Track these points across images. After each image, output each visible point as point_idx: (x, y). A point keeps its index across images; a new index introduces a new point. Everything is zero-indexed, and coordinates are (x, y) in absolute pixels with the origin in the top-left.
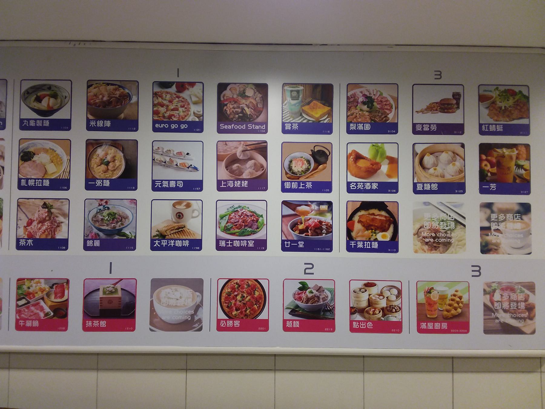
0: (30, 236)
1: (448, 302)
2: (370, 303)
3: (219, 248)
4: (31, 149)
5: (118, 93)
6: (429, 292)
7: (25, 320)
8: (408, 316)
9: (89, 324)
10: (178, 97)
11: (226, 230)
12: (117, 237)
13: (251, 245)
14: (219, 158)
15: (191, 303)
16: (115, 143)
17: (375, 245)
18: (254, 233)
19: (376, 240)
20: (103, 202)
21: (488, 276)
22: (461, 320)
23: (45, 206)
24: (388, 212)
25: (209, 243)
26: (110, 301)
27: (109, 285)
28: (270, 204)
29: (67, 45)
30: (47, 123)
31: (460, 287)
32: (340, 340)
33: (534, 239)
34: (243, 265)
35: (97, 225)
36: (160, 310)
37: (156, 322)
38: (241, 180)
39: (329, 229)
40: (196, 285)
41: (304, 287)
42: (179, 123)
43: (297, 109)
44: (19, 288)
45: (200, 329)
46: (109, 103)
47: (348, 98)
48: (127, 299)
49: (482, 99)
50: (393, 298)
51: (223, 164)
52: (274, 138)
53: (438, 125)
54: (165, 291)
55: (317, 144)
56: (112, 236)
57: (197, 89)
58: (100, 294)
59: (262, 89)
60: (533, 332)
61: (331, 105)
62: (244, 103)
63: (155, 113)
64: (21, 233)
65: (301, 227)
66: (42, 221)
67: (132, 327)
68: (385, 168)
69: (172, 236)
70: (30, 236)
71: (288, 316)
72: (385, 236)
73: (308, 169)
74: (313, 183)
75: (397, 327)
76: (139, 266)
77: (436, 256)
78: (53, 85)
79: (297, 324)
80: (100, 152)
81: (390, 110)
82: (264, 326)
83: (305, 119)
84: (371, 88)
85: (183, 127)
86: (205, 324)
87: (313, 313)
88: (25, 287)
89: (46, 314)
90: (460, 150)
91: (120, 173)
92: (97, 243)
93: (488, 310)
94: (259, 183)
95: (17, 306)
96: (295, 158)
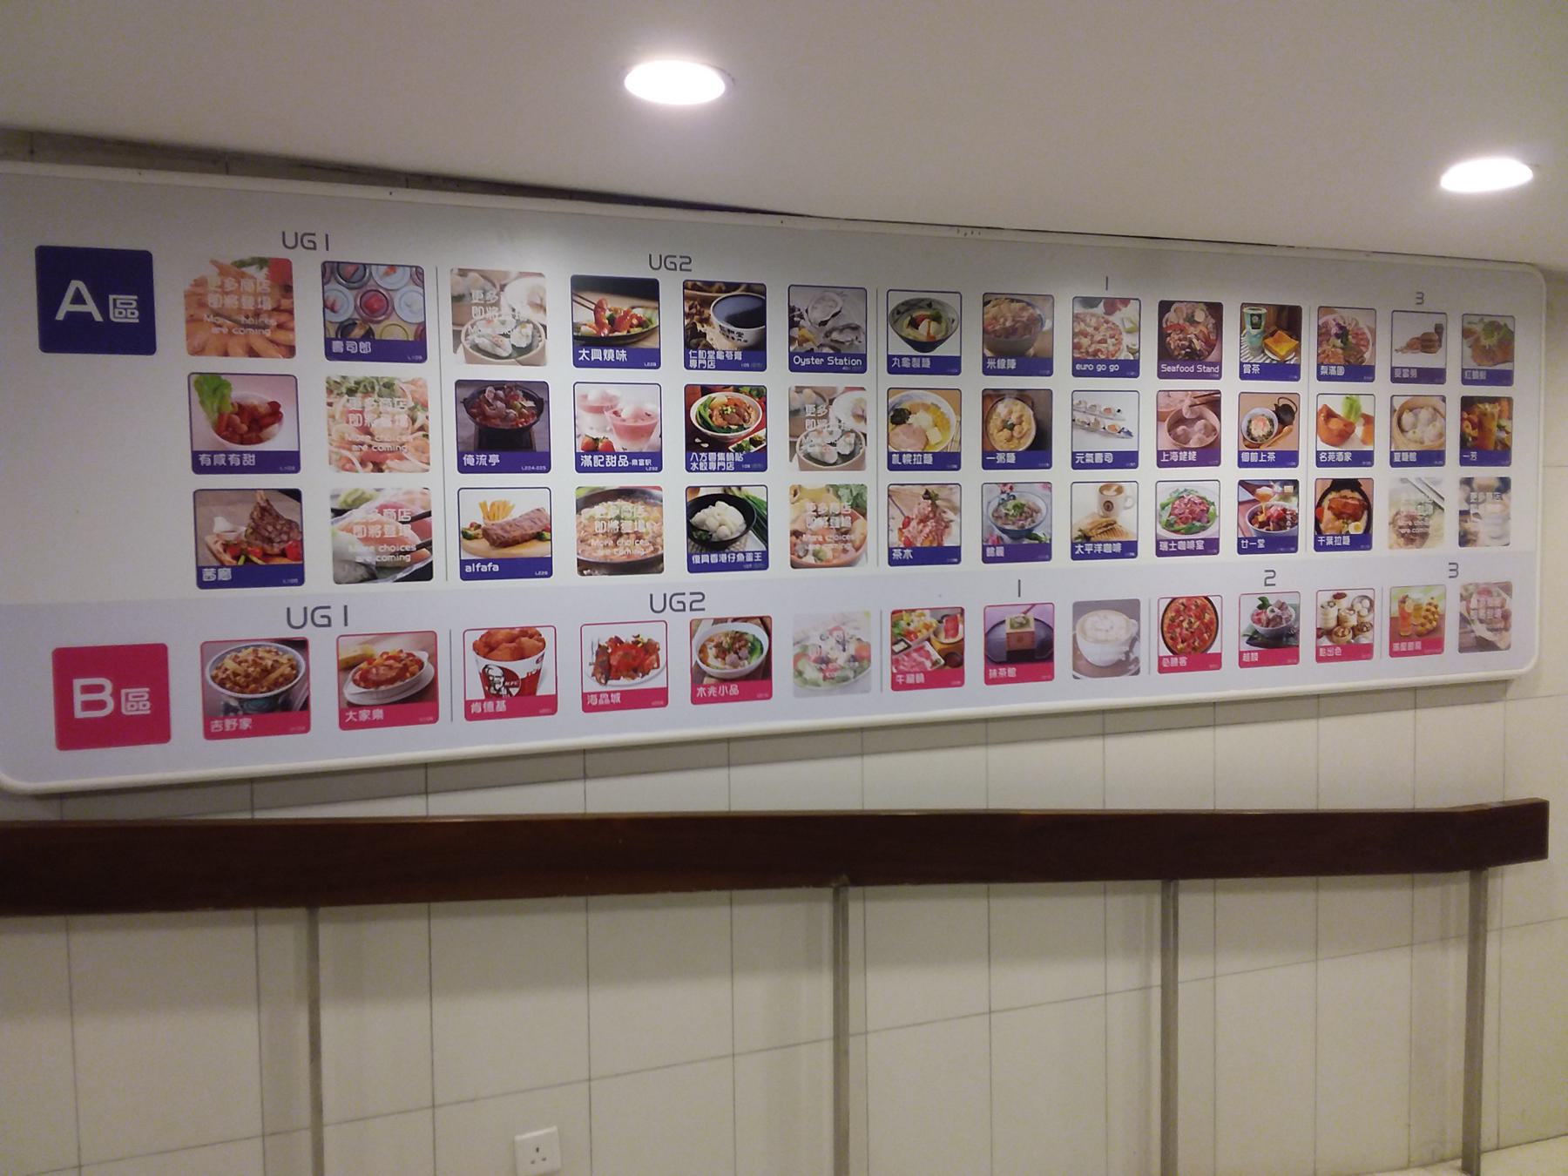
0: (908, 544)
1: (1424, 613)
2: (1340, 621)
3: (1160, 553)
4: (905, 406)
5: (1026, 314)
6: (1403, 601)
7: (904, 673)
8: (1379, 636)
9: (993, 673)
10: (1107, 322)
11: (1168, 526)
12: (1026, 541)
13: (1200, 547)
14: (1160, 417)
15: (1125, 636)
16: (1022, 396)
17: (1347, 541)
18: (1204, 528)
19: (1347, 533)
20: (1007, 488)
21: (1466, 577)
22: (1431, 637)
23: (927, 495)
24: (1362, 493)
25: (1146, 547)
26: (1020, 637)
27: (1017, 614)
28: (1222, 484)
29: (953, 233)
30: (927, 364)
31: (1435, 593)
32: (1307, 674)
33: (1514, 525)
34: (1190, 577)
35: (999, 523)
36: (1087, 649)
37: (1082, 667)
38: (1188, 450)
39: (1295, 517)
40: (1130, 608)
41: (1264, 605)
42: (1107, 362)
43: (1258, 342)
44: (894, 625)
45: (1137, 673)
46: (1012, 331)
47: (1319, 328)
48: (1042, 634)
49: (1466, 333)
50: (1364, 612)
51: (1165, 425)
52: (1230, 386)
53: (1420, 370)
54: (1091, 620)
55: (1282, 396)
56: (1020, 542)
57: (1129, 312)
58: (1007, 629)
59: (1215, 310)
60: (1508, 648)
61: (1298, 338)
62: (1192, 332)
63: (1076, 347)
64: (896, 540)
65: (1261, 518)
66: (924, 520)
67: (1049, 675)
68: (1359, 431)
69: (1100, 538)
70: (908, 544)
71: (1245, 647)
72: (1356, 528)
73: (1270, 433)
74: (1277, 453)
75: (1364, 652)
76: (1054, 585)
77: (1412, 552)
78: (939, 303)
79: (1255, 656)
80: (1001, 409)
81: (1366, 346)
82: (1215, 662)
83: (1269, 358)
84: (1345, 313)
85: (1113, 368)
86: (1143, 666)
87: (1274, 641)
88: (903, 624)
89: (935, 663)
90: (1440, 405)
91: (1029, 441)
92: (1000, 552)
93: (1464, 621)
94: (1209, 455)
95: (893, 652)
96: (1255, 416)
